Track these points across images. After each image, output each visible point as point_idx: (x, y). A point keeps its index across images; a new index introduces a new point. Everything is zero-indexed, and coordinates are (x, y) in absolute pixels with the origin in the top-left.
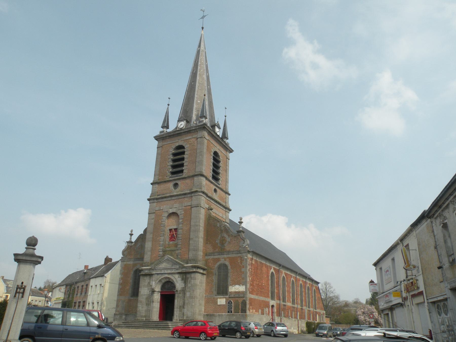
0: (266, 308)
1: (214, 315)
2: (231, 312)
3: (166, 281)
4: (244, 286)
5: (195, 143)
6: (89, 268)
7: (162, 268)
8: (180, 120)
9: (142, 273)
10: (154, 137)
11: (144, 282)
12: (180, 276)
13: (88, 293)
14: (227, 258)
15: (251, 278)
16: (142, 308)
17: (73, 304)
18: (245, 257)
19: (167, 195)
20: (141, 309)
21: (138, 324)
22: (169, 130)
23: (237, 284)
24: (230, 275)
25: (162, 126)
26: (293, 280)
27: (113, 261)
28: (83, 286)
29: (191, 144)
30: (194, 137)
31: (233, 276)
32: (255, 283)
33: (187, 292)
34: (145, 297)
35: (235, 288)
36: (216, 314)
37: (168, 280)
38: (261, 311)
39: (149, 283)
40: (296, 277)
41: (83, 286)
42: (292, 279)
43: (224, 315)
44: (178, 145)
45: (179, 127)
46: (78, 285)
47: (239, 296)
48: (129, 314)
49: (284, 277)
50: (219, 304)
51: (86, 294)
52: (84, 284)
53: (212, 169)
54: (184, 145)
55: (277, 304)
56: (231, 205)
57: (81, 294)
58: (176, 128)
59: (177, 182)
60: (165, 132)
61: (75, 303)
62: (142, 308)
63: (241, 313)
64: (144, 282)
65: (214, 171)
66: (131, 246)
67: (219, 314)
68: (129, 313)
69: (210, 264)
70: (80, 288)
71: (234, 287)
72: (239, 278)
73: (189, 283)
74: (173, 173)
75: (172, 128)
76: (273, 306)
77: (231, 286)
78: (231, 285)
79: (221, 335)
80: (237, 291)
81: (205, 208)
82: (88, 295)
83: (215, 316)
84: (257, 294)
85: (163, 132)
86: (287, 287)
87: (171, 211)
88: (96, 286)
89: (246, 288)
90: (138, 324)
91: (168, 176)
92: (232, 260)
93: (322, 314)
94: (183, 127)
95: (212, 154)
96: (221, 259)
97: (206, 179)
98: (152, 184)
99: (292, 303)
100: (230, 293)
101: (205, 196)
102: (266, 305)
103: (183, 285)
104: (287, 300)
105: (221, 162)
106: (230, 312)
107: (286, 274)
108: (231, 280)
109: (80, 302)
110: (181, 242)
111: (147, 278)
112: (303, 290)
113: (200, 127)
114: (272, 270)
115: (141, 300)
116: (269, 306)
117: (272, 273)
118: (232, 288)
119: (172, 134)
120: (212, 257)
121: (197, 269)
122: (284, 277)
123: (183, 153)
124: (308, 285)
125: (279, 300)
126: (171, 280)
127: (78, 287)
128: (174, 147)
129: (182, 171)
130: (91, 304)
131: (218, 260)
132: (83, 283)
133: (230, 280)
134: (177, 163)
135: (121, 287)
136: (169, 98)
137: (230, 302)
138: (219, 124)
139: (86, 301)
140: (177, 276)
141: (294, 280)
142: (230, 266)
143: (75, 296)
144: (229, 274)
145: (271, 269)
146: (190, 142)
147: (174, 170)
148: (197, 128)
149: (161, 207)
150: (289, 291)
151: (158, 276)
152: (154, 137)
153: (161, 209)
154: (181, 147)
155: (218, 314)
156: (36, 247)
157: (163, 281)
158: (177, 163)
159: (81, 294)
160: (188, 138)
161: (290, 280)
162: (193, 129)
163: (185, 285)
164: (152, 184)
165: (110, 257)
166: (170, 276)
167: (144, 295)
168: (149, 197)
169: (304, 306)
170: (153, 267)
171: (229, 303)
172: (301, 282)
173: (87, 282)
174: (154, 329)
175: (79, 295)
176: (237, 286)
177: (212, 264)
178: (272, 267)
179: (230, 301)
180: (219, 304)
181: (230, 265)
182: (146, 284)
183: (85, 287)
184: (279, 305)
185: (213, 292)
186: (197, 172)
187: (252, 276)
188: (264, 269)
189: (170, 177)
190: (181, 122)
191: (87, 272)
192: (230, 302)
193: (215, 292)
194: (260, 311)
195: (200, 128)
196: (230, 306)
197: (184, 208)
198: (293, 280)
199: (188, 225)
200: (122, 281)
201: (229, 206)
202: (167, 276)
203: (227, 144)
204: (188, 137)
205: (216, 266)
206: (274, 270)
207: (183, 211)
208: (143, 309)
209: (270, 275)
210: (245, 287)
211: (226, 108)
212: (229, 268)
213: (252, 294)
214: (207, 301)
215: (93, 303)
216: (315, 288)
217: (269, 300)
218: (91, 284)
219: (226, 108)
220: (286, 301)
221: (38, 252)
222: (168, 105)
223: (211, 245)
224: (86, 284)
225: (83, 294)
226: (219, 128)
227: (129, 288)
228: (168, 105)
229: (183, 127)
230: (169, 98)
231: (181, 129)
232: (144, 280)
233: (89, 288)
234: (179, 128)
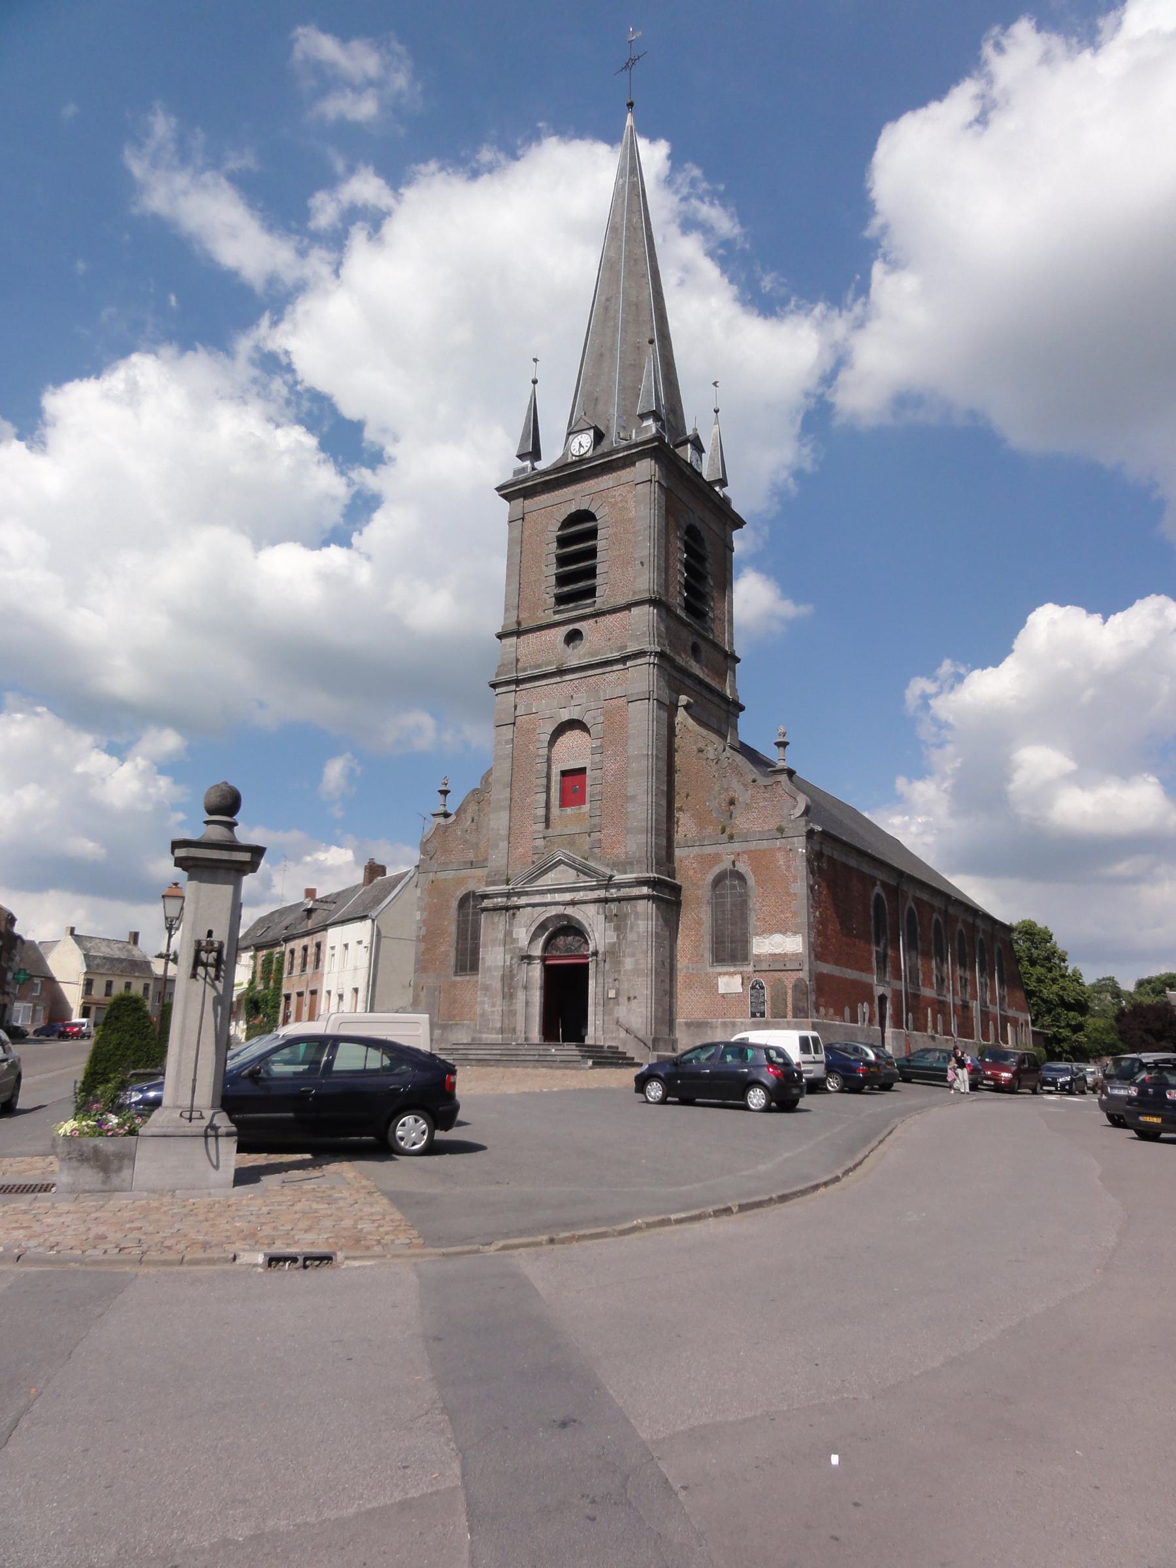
0: (863, 1005)
1: (708, 1023)
2: (762, 1015)
4: (797, 936)
5: (626, 502)
6: (318, 896)
7: (546, 888)
9: (486, 903)
11: (491, 929)
12: (601, 910)
13: (323, 965)
14: (744, 852)
15: (820, 912)
16: (493, 1005)
17: (283, 999)
18: (800, 850)
19: (549, 668)
20: (489, 1010)
21: (488, 1052)
22: (541, 465)
23: (776, 932)
24: (754, 903)
25: (519, 451)
26: (937, 920)
27: (390, 873)
28: (305, 949)
29: (616, 503)
31: (763, 906)
32: (830, 927)
33: (624, 956)
34: (498, 974)
35: (770, 944)
36: (714, 1020)
38: (851, 1012)
39: (509, 933)
40: (946, 911)
41: (305, 949)
42: (935, 916)
43: (739, 1024)
44: (573, 510)
45: (574, 453)
47: (785, 968)
48: (452, 1025)
49: (910, 909)
50: (721, 991)
51: (320, 969)
52: (310, 944)
57: (303, 970)
58: (565, 455)
59: (577, 626)
60: (529, 469)
61: (288, 997)
62: (493, 1005)
63: (793, 1017)
64: (493, 929)
65: (688, 586)
66: (447, 827)
67: (725, 1020)
68: (450, 1022)
69: (691, 873)
70: (299, 954)
72: (782, 912)
73: (632, 927)
75: (550, 457)
76: (883, 999)
77: (757, 937)
78: (757, 934)
79: (677, 1099)
80: (777, 951)
82: (323, 974)
83: (711, 1027)
84: (837, 962)
85: (524, 470)
86: (920, 940)
87: (565, 716)
88: (346, 946)
90: (488, 1052)
91: (545, 609)
92: (756, 858)
93: (1022, 1024)
94: (586, 453)
96: (724, 857)
97: (667, 614)
99: (935, 988)
100: (756, 958)
102: (865, 993)
103: (612, 937)
104: (923, 980)
105: (710, 560)
106: (758, 1015)
107: (918, 901)
108: (759, 919)
110: (600, 808)
111: (502, 918)
112: (967, 951)
114: (878, 889)
115: (488, 983)
116: (873, 997)
117: (878, 896)
118: (761, 944)
120: (695, 851)
122: (910, 909)
123: (592, 534)
124: (981, 936)
129: (591, 592)
130: (334, 999)
131: (716, 858)
132: (305, 941)
133: (755, 918)
135: (423, 946)
136: (535, 360)
137: (757, 986)
138: (697, 438)
139: (318, 991)
140: (592, 909)
141: (940, 920)
142: (753, 876)
143: (285, 976)
144: (751, 904)
145: (874, 885)
149: (532, 704)
153: (534, 711)
154: (585, 516)
155: (720, 1020)
156: (237, 817)
159: (303, 970)
160: (603, 486)
161: (930, 920)
163: (618, 937)
165: (378, 862)
166: (569, 911)
167: (496, 967)
170: (519, 886)
171: (753, 988)
172: (960, 926)
173: (318, 937)
174: (535, 1067)
175: (297, 971)
176: (778, 937)
177: (695, 872)
178: (876, 878)
179: (756, 981)
180: (721, 991)
181: (754, 873)
182: (501, 936)
183: (312, 950)
184: (897, 994)
185: (702, 956)
186: (640, 591)
187: (820, 907)
189: (556, 613)
190: (579, 437)
191: (316, 909)
192: (757, 986)
193: (708, 956)
194: (847, 1011)
197: (602, 703)
198: (937, 920)
199: (618, 756)
200: (427, 930)
201: (738, 697)
203: (726, 501)
204: (606, 481)
205: (710, 877)
206: (884, 890)
207: (602, 714)
208: (496, 1009)
209: (872, 903)
210: (801, 938)
212: (751, 881)
213: (825, 961)
214: (685, 982)
215: (341, 997)
216: (1001, 946)
220: (920, 983)
221: (246, 833)
222: (535, 382)
223: (692, 816)
225: (310, 969)
226: (699, 450)
227: (448, 948)
228: (535, 382)
229: (588, 451)
230: (535, 360)
231: (582, 460)
232: (493, 923)
233: (324, 952)
234: (573, 455)
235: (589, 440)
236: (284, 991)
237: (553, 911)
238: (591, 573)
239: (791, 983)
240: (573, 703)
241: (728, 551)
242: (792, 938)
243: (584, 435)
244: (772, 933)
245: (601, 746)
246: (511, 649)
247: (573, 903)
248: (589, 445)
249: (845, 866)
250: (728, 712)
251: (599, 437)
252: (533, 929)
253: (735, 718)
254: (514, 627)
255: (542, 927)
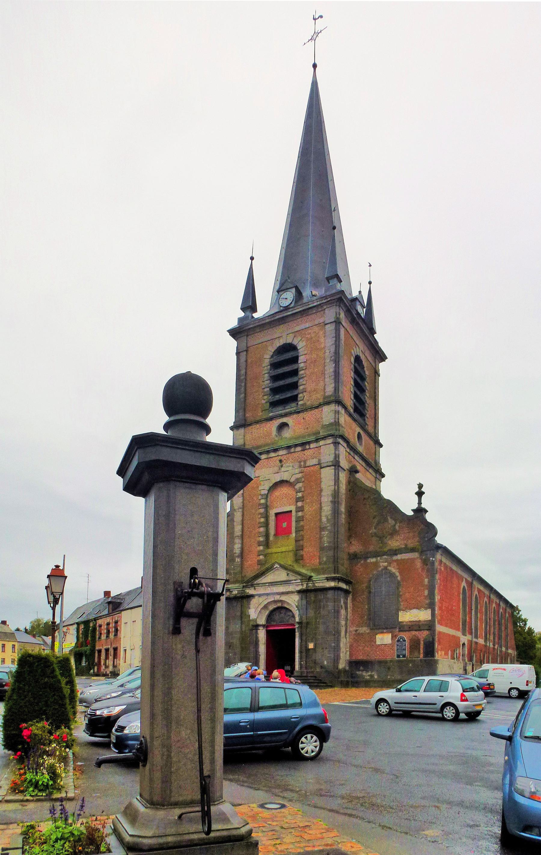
3: (275, 607)
4: (428, 610)
8: (282, 288)
10: (228, 331)
12: (303, 596)
17: (97, 652)
18: (431, 559)
30: (316, 322)
34: (238, 636)
37: (279, 605)
40: (490, 597)
41: (108, 624)
46: (99, 622)
50: (378, 642)
53: (353, 393)
54: (295, 343)
55: (468, 640)
56: (385, 466)
57: (108, 636)
59: (284, 420)
61: (100, 651)
65: (356, 396)
70: (104, 627)
71: (408, 613)
74: (274, 404)
81: (346, 469)
87: (278, 478)
89: (433, 615)
94: (290, 304)
95: (353, 360)
98: (232, 428)
101: (345, 445)
106: (401, 656)
107: (479, 591)
109: (107, 650)
113: (329, 299)
119: (268, 321)
121: (338, 583)
122: (476, 595)
123: (295, 360)
125: (471, 633)
126: (286, 606)
127: (100, 626)
128: (272, 349)
129: (295, 399)
132: (108, 620)
134: (281, 383)
146: (308, 335)
147: (277, 397)
148: (324, 301)
150: (481, 619)
151: (261, 599)
152: (228, 331)
154: (289, 348)
157: (271, 608)
158: (281, 383)
159: (108, 636)
160: (302, 326)
162: (315, 304)
164: (232, 428)
166: (283, 598)
168: (49, 574)
169: (77, 675)
171: (398, 641)
175: (104, 637)
176: (415, 611)
178: (463, 577)
180: (378, 642)
184: (470, 642)
188: (455, 580)
192: (401, 640)
195: (329, 301)
196: (402, 646)
202: (277, 597)
211: (370, 266)
217: (459, 634)
218: (123, 621)
219: (370, 266)
224: (114, 621)
225: (112, 636)
229: (291, 303)
235: (292, 296)
236: (97, 648)
237: (271, 599)
238: (295, 386)
239: (423, 637)
240: (283, 469)
241: (377, 376)
242: (425, 611)
243: (288, 293)
244: (411, 609)
245: (303, 497)
246: (240, 437)
247: (283, 593)
248: (292, 299)
249: (451, 569)
250: (376, 478)
251: (299, 295)
252: (259, 609)
253: (379, 481)
254: (243, 422)
255: (265, 607)
